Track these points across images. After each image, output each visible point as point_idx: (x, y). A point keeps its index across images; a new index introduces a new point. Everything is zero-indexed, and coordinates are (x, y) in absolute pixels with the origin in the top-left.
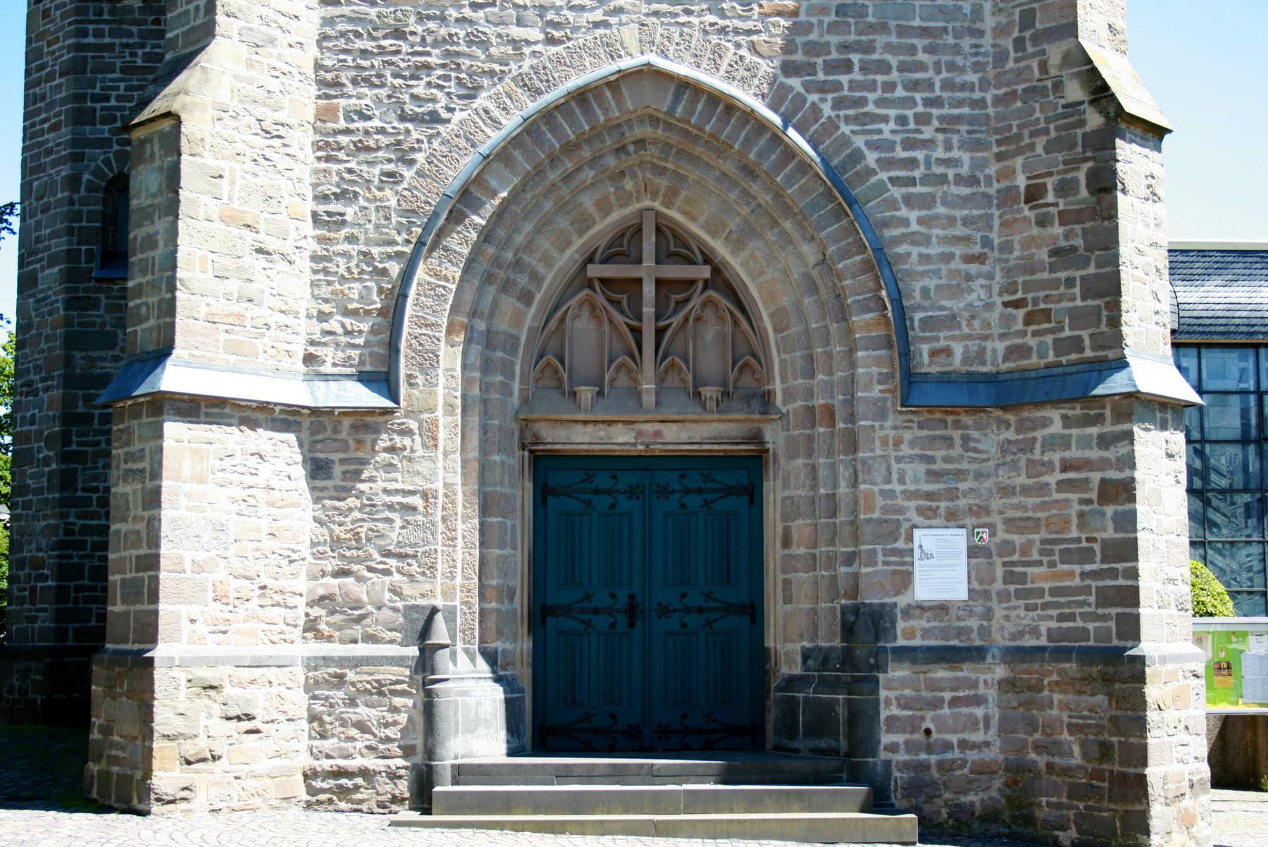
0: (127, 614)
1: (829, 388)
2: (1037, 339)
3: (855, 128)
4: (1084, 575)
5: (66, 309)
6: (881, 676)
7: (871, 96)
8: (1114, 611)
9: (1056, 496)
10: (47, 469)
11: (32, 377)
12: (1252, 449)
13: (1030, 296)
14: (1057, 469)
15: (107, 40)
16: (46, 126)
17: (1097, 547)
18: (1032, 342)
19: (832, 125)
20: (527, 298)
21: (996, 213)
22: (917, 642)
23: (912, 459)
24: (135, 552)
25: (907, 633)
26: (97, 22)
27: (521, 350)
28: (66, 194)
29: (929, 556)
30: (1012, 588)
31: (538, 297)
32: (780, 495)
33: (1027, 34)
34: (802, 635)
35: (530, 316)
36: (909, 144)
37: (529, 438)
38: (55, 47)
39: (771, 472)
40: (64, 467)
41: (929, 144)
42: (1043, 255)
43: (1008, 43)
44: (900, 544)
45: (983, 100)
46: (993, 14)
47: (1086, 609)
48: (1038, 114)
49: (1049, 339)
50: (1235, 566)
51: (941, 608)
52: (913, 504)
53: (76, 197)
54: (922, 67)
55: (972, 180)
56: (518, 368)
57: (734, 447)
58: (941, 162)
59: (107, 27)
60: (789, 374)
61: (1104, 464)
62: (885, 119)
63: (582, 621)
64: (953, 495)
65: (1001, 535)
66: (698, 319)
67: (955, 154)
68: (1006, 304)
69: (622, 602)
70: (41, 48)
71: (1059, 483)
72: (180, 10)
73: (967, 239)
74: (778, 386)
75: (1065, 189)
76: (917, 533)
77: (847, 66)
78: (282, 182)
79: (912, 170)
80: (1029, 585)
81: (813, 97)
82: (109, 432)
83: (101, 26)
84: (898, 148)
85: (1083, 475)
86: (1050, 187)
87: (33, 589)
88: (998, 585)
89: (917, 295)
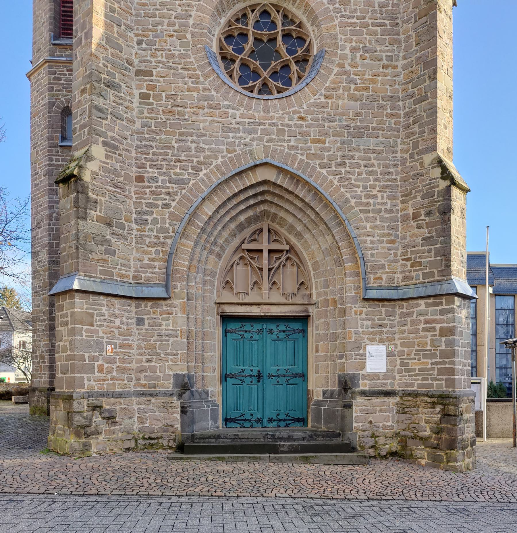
0: (63, 377)
1: (333, 292)
2: (415, 273)
3: (346, 190)
4: (432, 364)
5: (49, 264)
6: (354, 401)
7: (353, 177)
8: (444, 377)
9: (422, 334)
10: (44, 323)
11: (38, 289)
13: (413, 256)
14: (422, 323)
15: (60, 163)
16: (39, 195)
17: (438, 353)
18: (413, 274)
19: (338, 189)
20: (219, 256)
21: (400, 224)
22: (367, 388)
23: (366, 319)
24: (65, 354)
25: (364, 385)
26: (57, 156)
27: (217, 277)
28: (47, 221)
29: (372, 356)
30: (403, 368)
31: (223, 257)
32: (315, 332)
33: (415, 151)
34: (323, 385)
35: (220, 264)
36: (368, 197)
37: (220, 311)
38: (41, 165)
39: (311, 324)
40: (50, 322)
41: (376, 196)
42: (419, 240)
43: (407, 156)
44: (361, 352)
45: (396, 179)
46: (401, 144)
47: (433, 376)
48: (418, 184)
49: (420, 273)
51: (375, 376)
52: (366, 336)
53: (51, 222)
54: (374, 165)
55: (391, 211)
56: (216, 284)
57: (298, 315)
58: (379, 204)
59: (60, 158)
60: (319, 286)
61: (442, 321)
62: (358, 187)
63: (241, 380)
64: (381, 333)
65: (399, 348)
66: (284, 265)
67: (385, 200)
68: (403, 260)
69: (255, 373)
70: (36, 166)
71: (423, 328)
72: (78, 133)
73: (389, 234)
74: (314, 292)
75: (429, 214)
76: (368, 347)
77: (344, 164)
78: (122, 207)
79: (368, 207)
80: (410, 367)
81: (330, 177)
83: (58, 157)
84: (363, 198)
85: (433, 325)
86: (422, 213)
87: (41, 366)
88: (398, 367)
89: (369, 256)
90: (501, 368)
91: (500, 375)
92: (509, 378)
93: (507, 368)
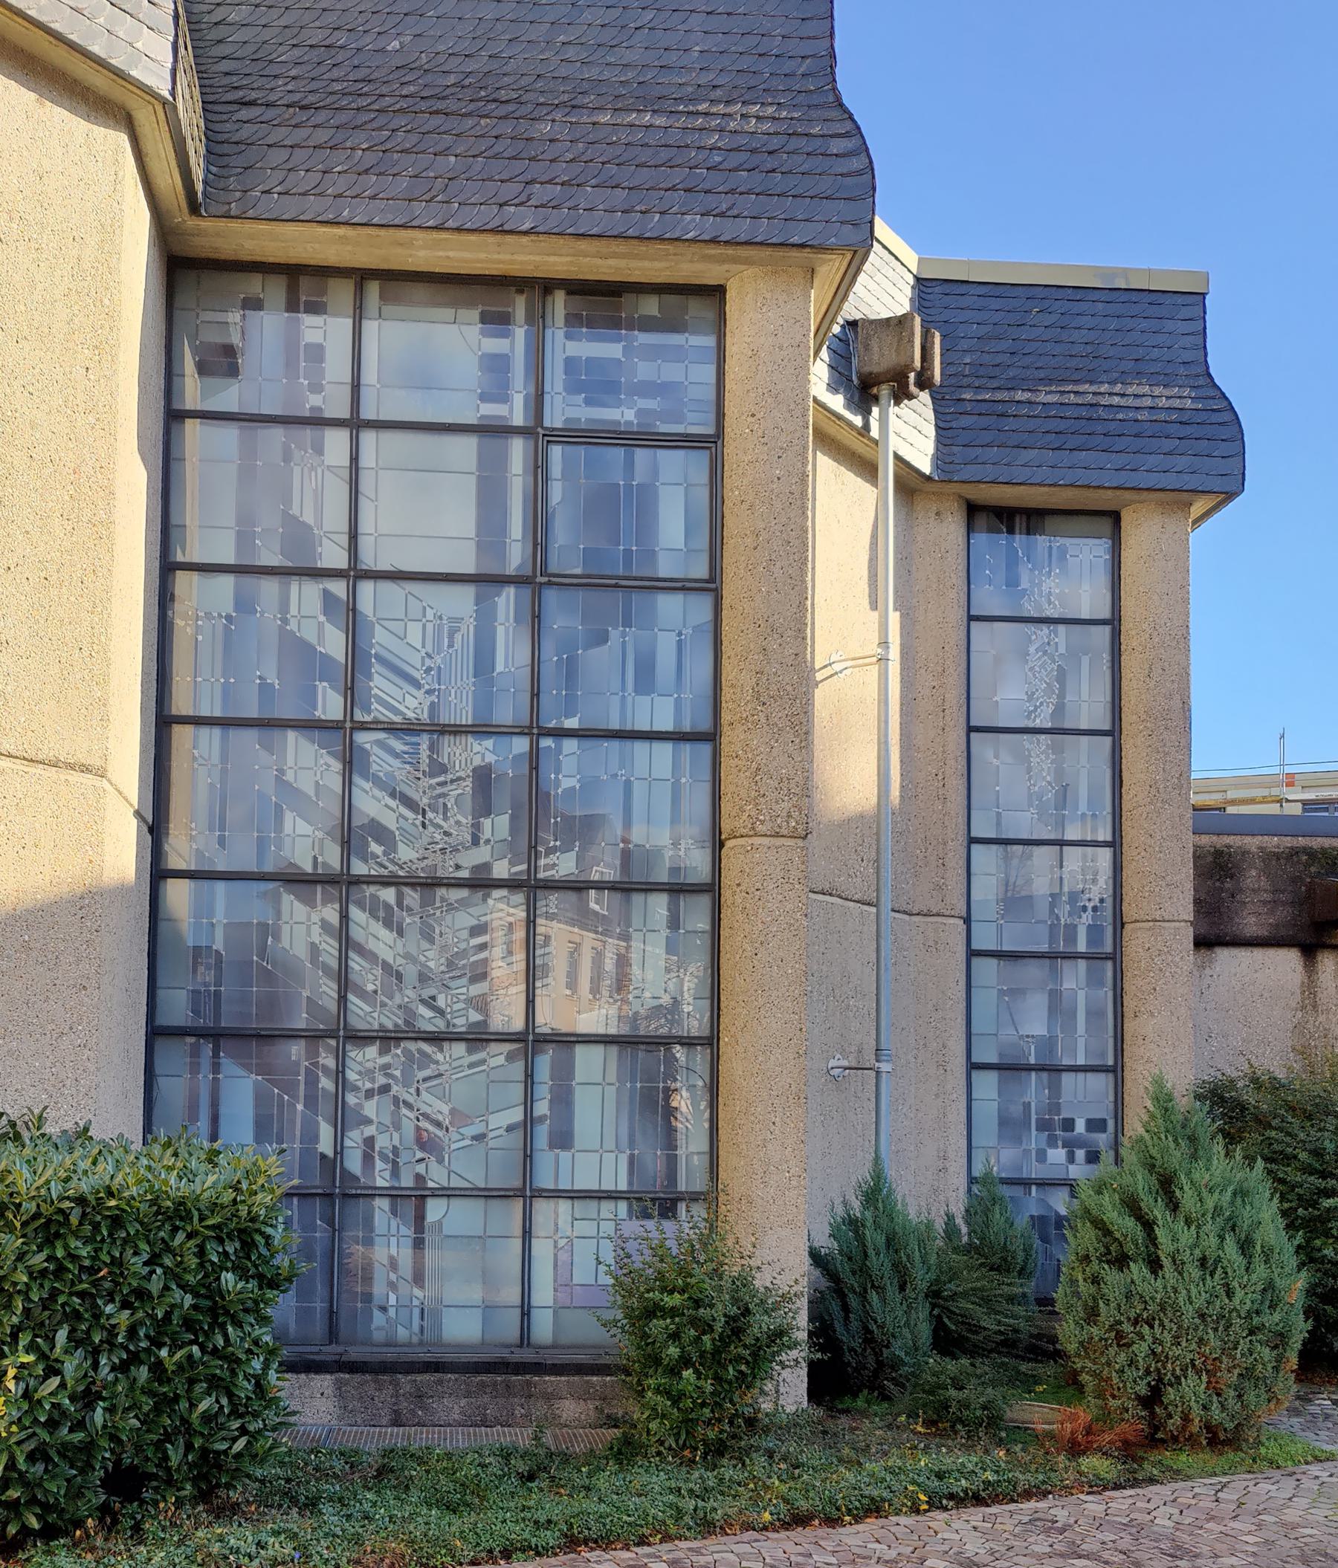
12: (507, 599)
50: (434, 962)
82: (197, 949)
90: (1010, 1068)
91: (1004, 1122)
92: (1070, 1146)
93: (1057, 1070)
